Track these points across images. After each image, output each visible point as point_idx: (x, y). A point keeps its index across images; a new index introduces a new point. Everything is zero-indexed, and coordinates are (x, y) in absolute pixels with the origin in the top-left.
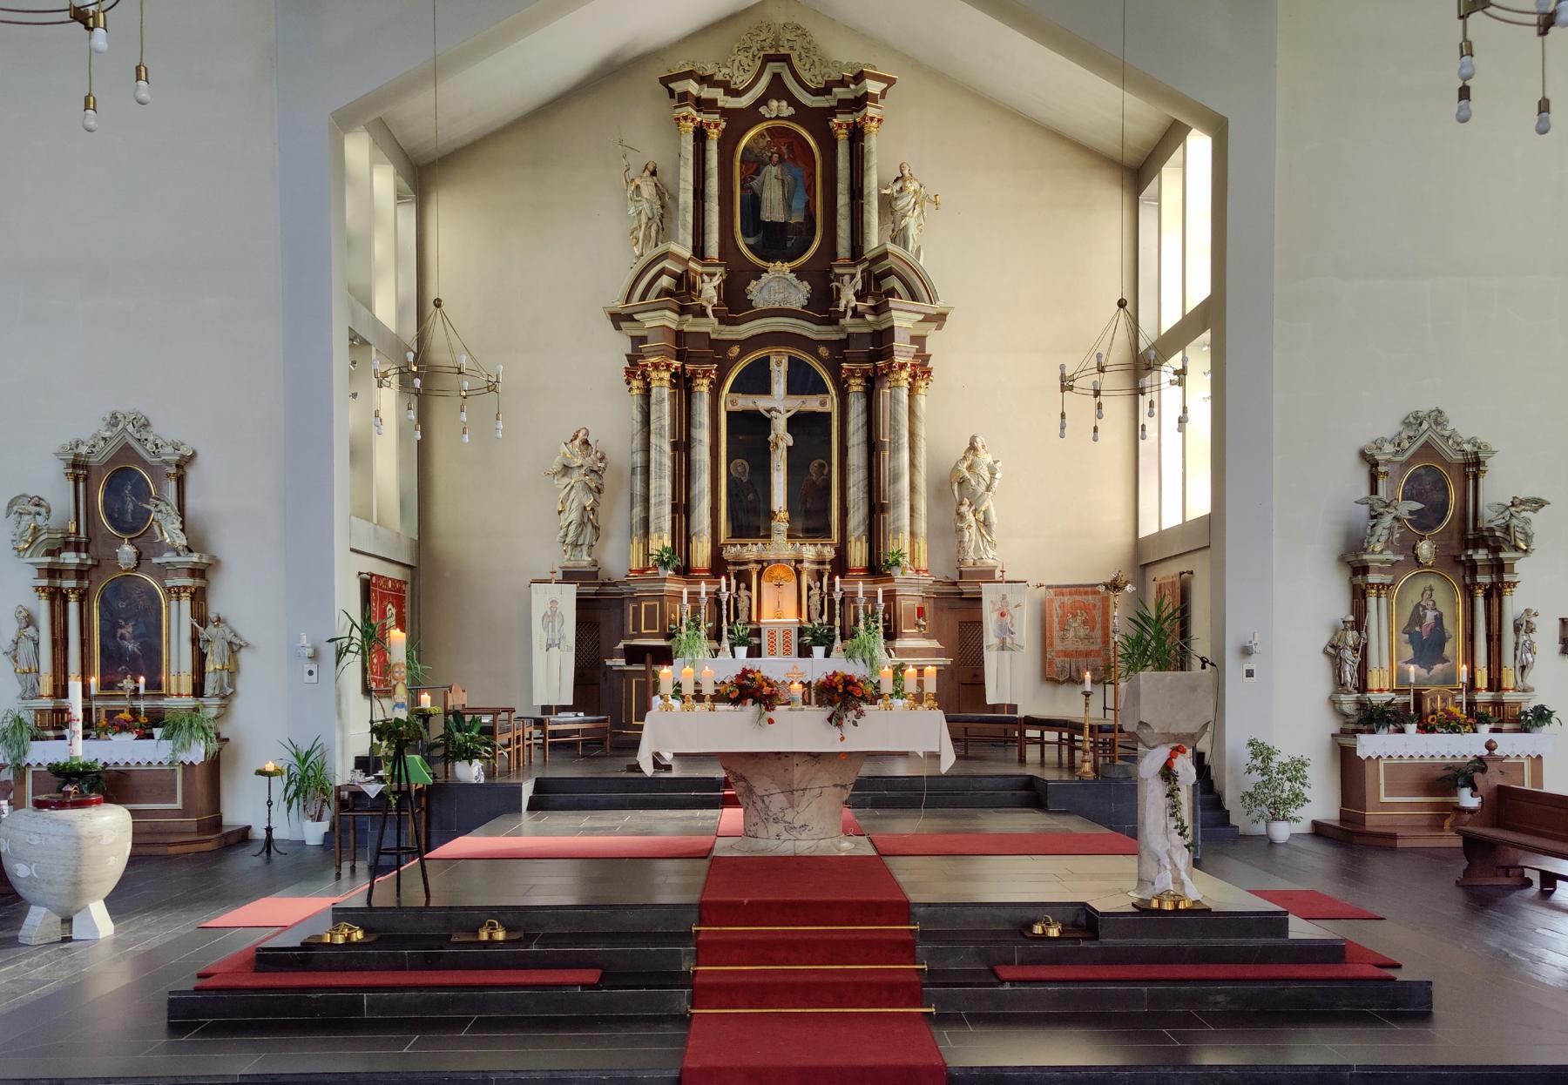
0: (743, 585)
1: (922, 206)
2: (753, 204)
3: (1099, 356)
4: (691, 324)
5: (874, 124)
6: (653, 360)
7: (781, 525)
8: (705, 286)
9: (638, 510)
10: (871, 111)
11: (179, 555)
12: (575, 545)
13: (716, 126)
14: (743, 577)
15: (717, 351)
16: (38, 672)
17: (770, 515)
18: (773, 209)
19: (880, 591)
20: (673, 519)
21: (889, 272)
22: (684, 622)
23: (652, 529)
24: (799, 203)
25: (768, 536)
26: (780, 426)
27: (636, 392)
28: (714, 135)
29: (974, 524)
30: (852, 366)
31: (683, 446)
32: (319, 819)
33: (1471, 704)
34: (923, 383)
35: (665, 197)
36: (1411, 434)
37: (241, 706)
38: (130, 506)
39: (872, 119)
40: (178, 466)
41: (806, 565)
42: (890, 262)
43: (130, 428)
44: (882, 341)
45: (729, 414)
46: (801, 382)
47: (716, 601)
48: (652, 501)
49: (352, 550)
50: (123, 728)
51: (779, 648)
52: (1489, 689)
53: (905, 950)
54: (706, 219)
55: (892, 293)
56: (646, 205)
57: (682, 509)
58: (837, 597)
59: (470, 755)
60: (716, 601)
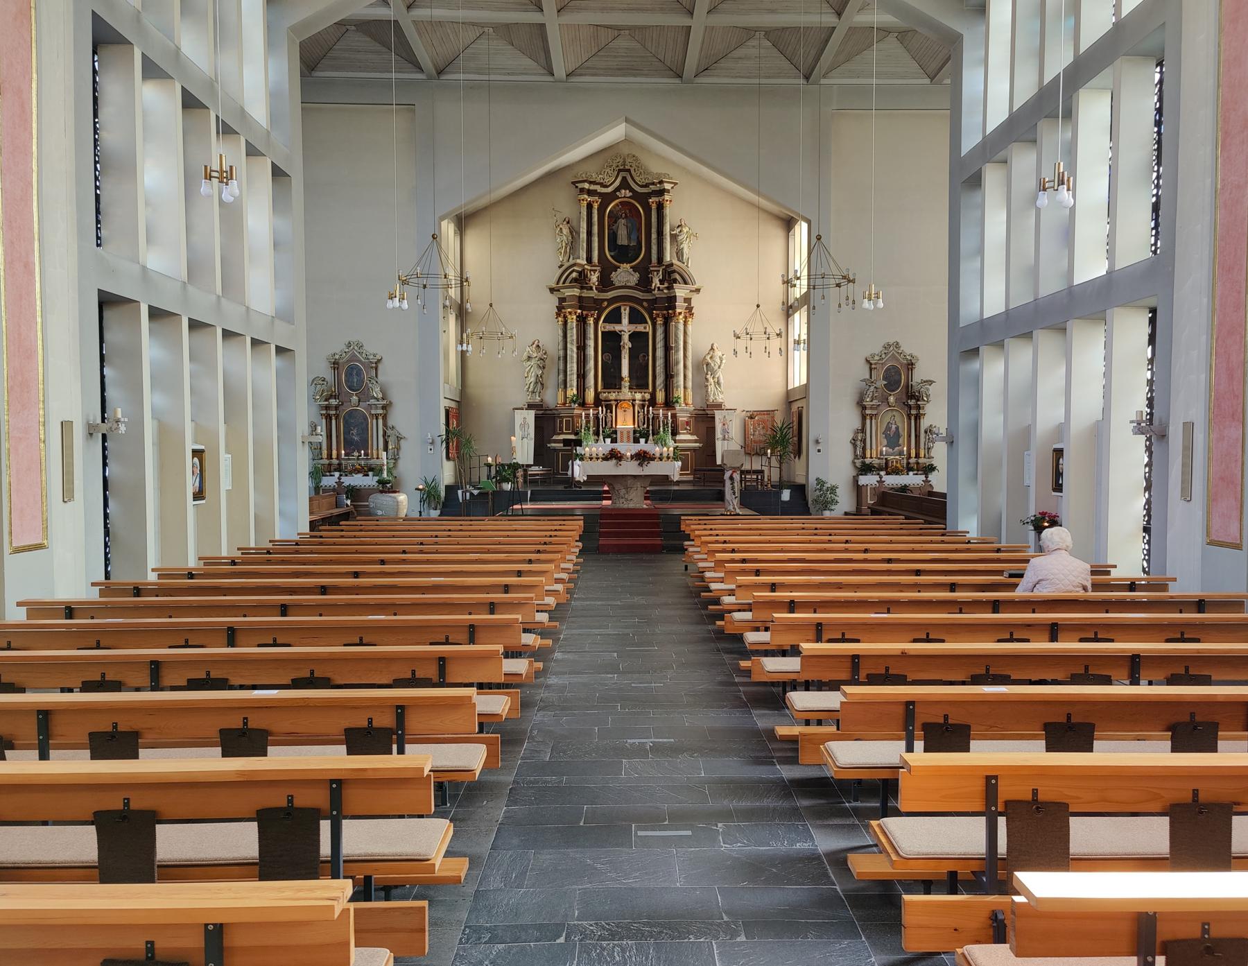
0: (609, 411)
1: (690, 238)
2: (613, 237)
3: (746, 329)
4: (586, 294)
5: (668, 202)
6: (569, 310)
7: (626, 384)
8: (592, 277)
9: (561, 376)
10: (667, 197)
11: (378, 401)
12: (533, 392)
13: (597, 202)
14: (609, 407)
15: (597, 305)
16: (321, 449)
17: (622, 379)
18: (623, 240)
19: (669, 414)
20: (578, 381)
21: (674, 271)
22: (583, 427)
23: (568, 386)
24: (634, 237)
25: (620, 388)
26: (626, 338)
27: (560, 323)
28: (596, 206)
29: (713, 383)
30: (658, 312)
31: (582, 348)
32: (436, 509)
33: (908, 463)
34: (690, 320)
35: (574, 232)
36: (886, 352)
37: (401, 462)
38: (355, 380)
39: (667, 201)
40: (376, 363)
41: (637, 402)
42: (675, 267)
43: (356, 348)
44: (672, 300)
45: (602, 332)
46: (635, 318)
47: (597, 417)
48: (568, 373)
49: (445, 398)
50: (359, 472)
51: (625, 439)
52: (327, 458)
53: (657, 525)
54: (592, 245)
55: (675, 281)
56: (565, 238)
57: (582, 376)
58: (651, 416)
59: (507, 481)
60: (597, 417)
